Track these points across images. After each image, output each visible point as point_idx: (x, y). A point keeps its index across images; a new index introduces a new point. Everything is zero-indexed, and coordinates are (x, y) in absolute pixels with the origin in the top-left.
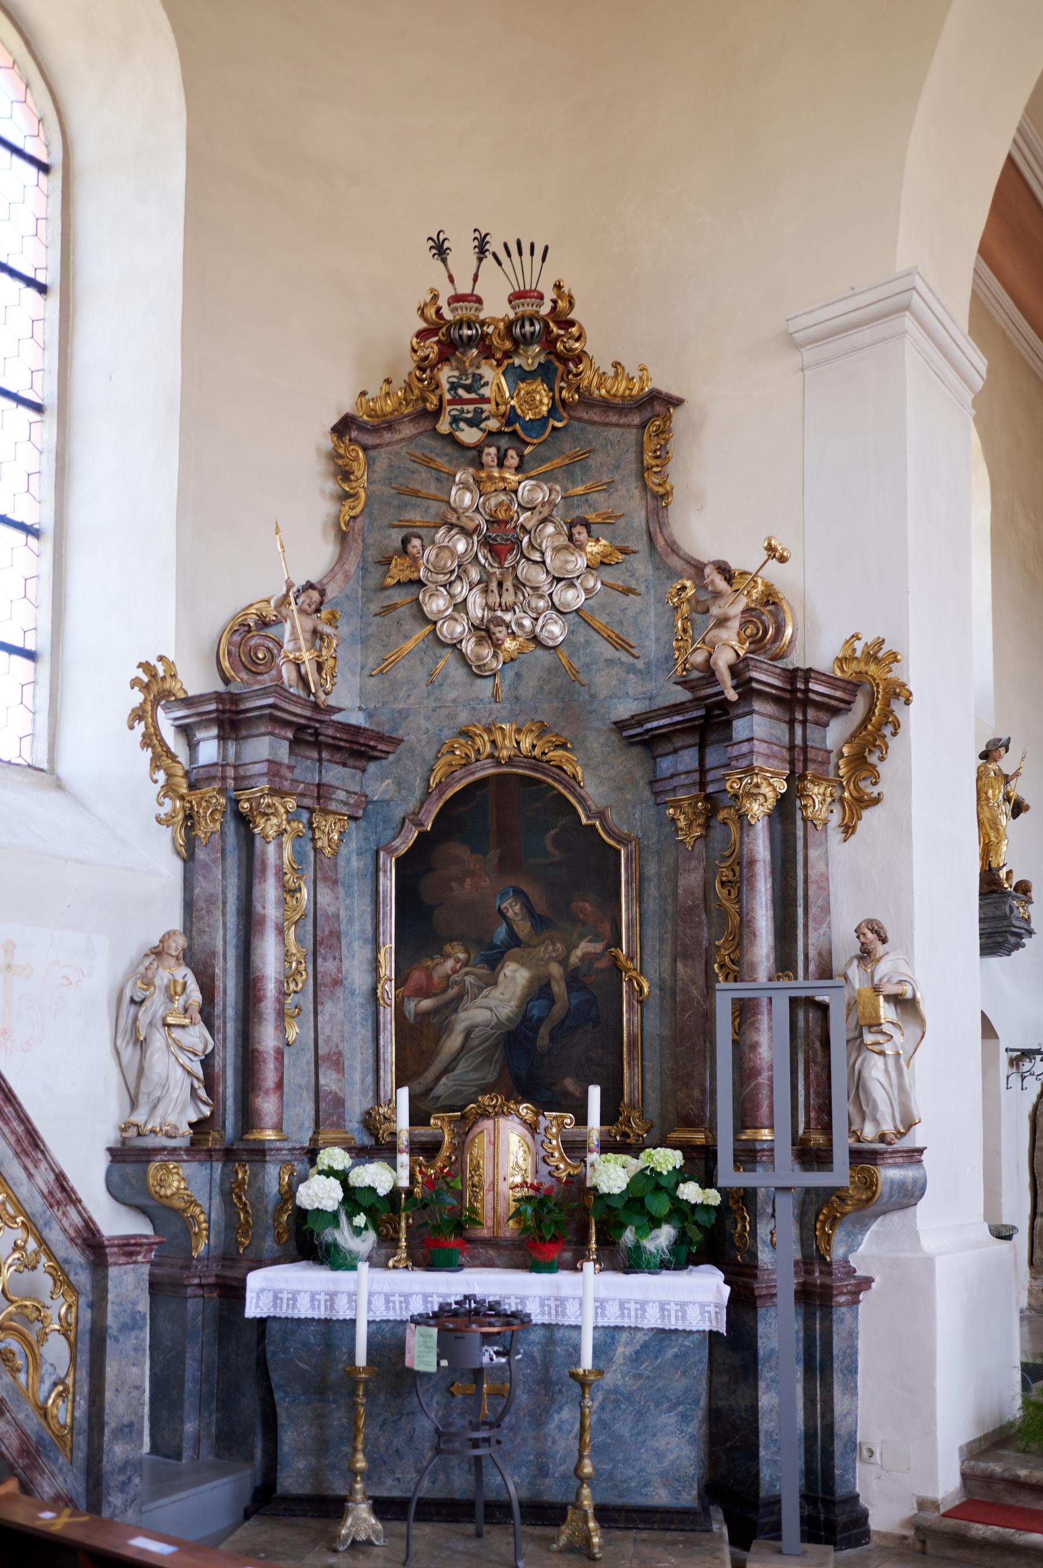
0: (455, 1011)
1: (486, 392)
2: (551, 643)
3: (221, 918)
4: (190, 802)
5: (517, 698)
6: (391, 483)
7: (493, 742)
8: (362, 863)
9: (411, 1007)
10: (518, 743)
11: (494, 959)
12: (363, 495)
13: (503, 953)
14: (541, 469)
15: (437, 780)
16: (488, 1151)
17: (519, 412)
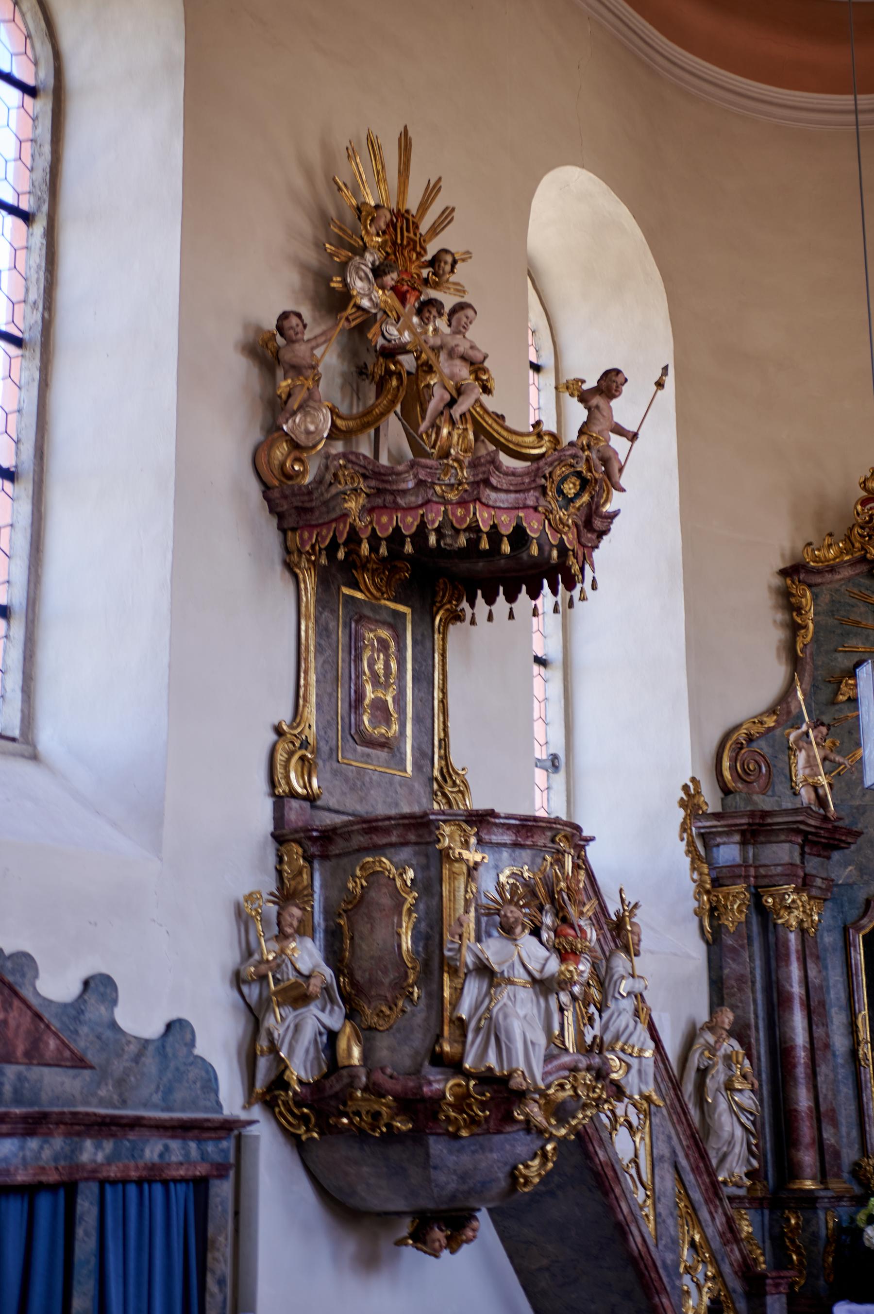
3: (751, 995)
4: (717, 897)
6: (833, 615)
8: (831, 939)
12: (811, 626)
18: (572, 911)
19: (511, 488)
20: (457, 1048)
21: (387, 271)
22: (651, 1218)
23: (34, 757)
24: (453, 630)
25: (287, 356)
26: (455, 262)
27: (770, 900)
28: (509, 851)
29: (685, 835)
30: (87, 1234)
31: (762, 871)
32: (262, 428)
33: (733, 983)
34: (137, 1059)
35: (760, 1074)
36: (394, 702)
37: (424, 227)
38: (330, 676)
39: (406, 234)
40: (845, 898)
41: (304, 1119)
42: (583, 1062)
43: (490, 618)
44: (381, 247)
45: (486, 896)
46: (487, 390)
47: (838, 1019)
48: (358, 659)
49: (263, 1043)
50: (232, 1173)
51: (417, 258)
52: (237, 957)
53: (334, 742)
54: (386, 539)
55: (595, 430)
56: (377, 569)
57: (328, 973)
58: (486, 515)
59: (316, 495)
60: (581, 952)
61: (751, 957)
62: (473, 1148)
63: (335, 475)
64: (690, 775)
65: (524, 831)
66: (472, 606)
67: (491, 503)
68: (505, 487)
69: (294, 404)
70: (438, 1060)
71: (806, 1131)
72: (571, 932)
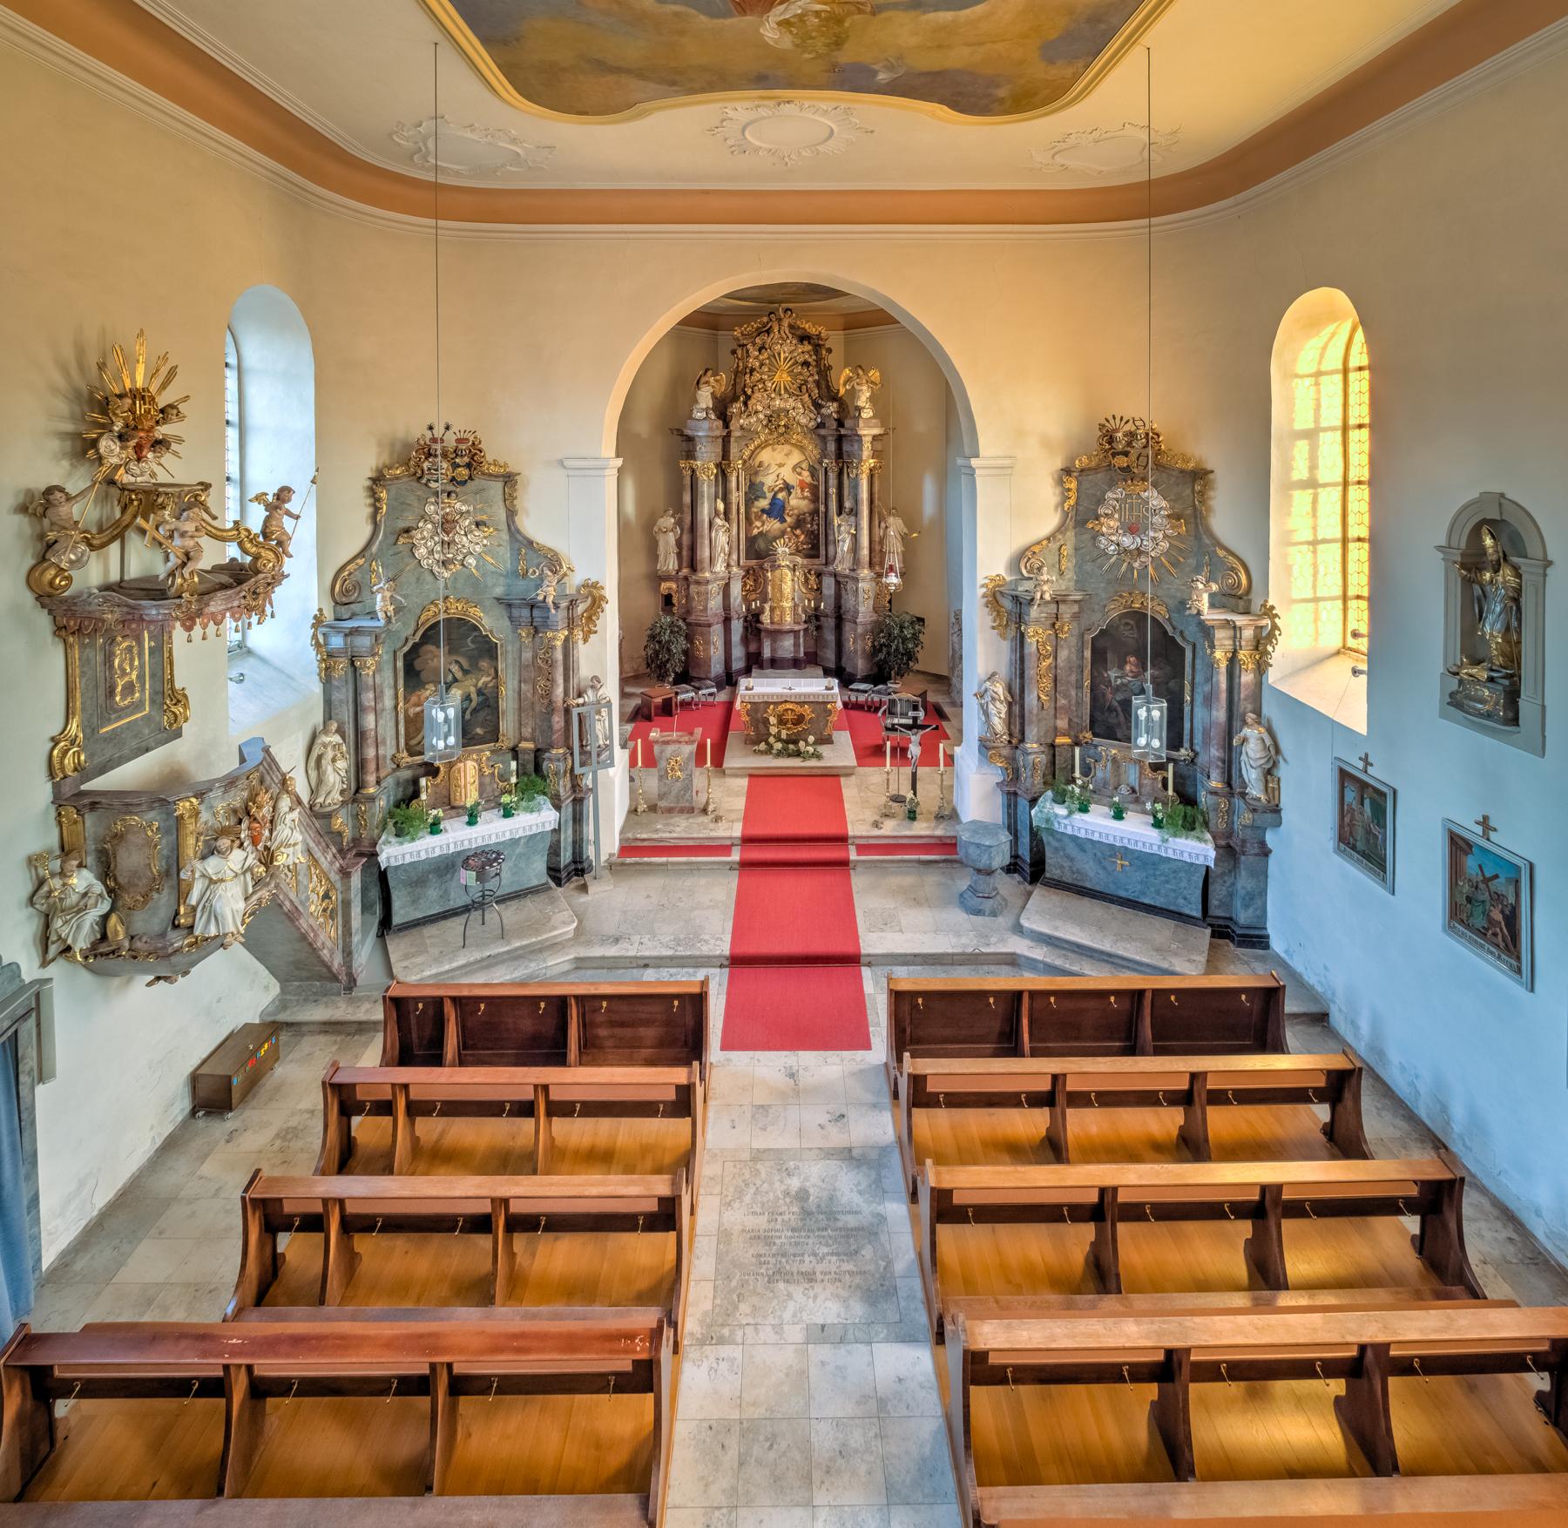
9: (412, 711)
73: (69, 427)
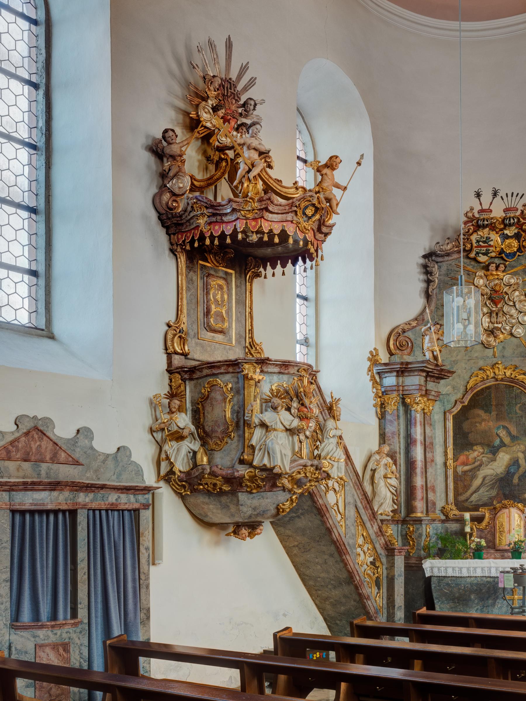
0: (479, 470)
1: (492, 243)
2: (518, 336)
5: (503, 356)
7: (494, 373)
9: (460, 469)
10: (505, 373)
11: (494, 451)
12: (437, 281)
13: (498, 449)
14: (512, 271)
15: (470, 386)
16: (506, 520)
17: (505, 250)
18: (306, 401)
19: (280, 212)
20: (251, 457)
21: (219, 108)
22: (343, 526)
23: (52, 337)
24: (256, 281)
25: (167, 151)
26: (255, 105)
27: (409, 400)
28: (277, 375)
29: (370, 373)
30: (82, 529)
31: (406, 388)
32: (157, 186)
33: (390, 435)
34: (104, 462)
35: (400, 472)
36: (226, 313)
37: (239, 87)
38: (194, 301)
39: (229, 90)
40: (445, 400)
41: (184, 487)
42: (309, 463)
43: (273, 275)
44: (216, 98)
45: (265, 394)
46: (270, 167)
47: (439, 450)
48: (208, 293)
49: (163, 456)
50: (151, 507)
51: (236, 103)
52: (151, 422)
53: (196, 331)
54: (218, 237)
55: (325, 185)
56: (217, 253)
57: (193, 428)
58: (266, 225)
59: (183, 217)
60: (310, 418)
61: (399, 424)
62: (259, 497)
63: (192, 207)
64: (374, 347)
65: (284, 367)
66: (265, 270)
67: (269, 219)
68: (276, 211)
69: (171, 174)
70: (242, 462)
71: (419, 494)
72: (306, 410)
73: (182, 105)
